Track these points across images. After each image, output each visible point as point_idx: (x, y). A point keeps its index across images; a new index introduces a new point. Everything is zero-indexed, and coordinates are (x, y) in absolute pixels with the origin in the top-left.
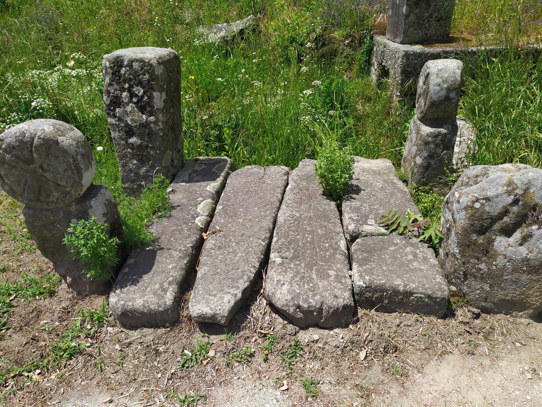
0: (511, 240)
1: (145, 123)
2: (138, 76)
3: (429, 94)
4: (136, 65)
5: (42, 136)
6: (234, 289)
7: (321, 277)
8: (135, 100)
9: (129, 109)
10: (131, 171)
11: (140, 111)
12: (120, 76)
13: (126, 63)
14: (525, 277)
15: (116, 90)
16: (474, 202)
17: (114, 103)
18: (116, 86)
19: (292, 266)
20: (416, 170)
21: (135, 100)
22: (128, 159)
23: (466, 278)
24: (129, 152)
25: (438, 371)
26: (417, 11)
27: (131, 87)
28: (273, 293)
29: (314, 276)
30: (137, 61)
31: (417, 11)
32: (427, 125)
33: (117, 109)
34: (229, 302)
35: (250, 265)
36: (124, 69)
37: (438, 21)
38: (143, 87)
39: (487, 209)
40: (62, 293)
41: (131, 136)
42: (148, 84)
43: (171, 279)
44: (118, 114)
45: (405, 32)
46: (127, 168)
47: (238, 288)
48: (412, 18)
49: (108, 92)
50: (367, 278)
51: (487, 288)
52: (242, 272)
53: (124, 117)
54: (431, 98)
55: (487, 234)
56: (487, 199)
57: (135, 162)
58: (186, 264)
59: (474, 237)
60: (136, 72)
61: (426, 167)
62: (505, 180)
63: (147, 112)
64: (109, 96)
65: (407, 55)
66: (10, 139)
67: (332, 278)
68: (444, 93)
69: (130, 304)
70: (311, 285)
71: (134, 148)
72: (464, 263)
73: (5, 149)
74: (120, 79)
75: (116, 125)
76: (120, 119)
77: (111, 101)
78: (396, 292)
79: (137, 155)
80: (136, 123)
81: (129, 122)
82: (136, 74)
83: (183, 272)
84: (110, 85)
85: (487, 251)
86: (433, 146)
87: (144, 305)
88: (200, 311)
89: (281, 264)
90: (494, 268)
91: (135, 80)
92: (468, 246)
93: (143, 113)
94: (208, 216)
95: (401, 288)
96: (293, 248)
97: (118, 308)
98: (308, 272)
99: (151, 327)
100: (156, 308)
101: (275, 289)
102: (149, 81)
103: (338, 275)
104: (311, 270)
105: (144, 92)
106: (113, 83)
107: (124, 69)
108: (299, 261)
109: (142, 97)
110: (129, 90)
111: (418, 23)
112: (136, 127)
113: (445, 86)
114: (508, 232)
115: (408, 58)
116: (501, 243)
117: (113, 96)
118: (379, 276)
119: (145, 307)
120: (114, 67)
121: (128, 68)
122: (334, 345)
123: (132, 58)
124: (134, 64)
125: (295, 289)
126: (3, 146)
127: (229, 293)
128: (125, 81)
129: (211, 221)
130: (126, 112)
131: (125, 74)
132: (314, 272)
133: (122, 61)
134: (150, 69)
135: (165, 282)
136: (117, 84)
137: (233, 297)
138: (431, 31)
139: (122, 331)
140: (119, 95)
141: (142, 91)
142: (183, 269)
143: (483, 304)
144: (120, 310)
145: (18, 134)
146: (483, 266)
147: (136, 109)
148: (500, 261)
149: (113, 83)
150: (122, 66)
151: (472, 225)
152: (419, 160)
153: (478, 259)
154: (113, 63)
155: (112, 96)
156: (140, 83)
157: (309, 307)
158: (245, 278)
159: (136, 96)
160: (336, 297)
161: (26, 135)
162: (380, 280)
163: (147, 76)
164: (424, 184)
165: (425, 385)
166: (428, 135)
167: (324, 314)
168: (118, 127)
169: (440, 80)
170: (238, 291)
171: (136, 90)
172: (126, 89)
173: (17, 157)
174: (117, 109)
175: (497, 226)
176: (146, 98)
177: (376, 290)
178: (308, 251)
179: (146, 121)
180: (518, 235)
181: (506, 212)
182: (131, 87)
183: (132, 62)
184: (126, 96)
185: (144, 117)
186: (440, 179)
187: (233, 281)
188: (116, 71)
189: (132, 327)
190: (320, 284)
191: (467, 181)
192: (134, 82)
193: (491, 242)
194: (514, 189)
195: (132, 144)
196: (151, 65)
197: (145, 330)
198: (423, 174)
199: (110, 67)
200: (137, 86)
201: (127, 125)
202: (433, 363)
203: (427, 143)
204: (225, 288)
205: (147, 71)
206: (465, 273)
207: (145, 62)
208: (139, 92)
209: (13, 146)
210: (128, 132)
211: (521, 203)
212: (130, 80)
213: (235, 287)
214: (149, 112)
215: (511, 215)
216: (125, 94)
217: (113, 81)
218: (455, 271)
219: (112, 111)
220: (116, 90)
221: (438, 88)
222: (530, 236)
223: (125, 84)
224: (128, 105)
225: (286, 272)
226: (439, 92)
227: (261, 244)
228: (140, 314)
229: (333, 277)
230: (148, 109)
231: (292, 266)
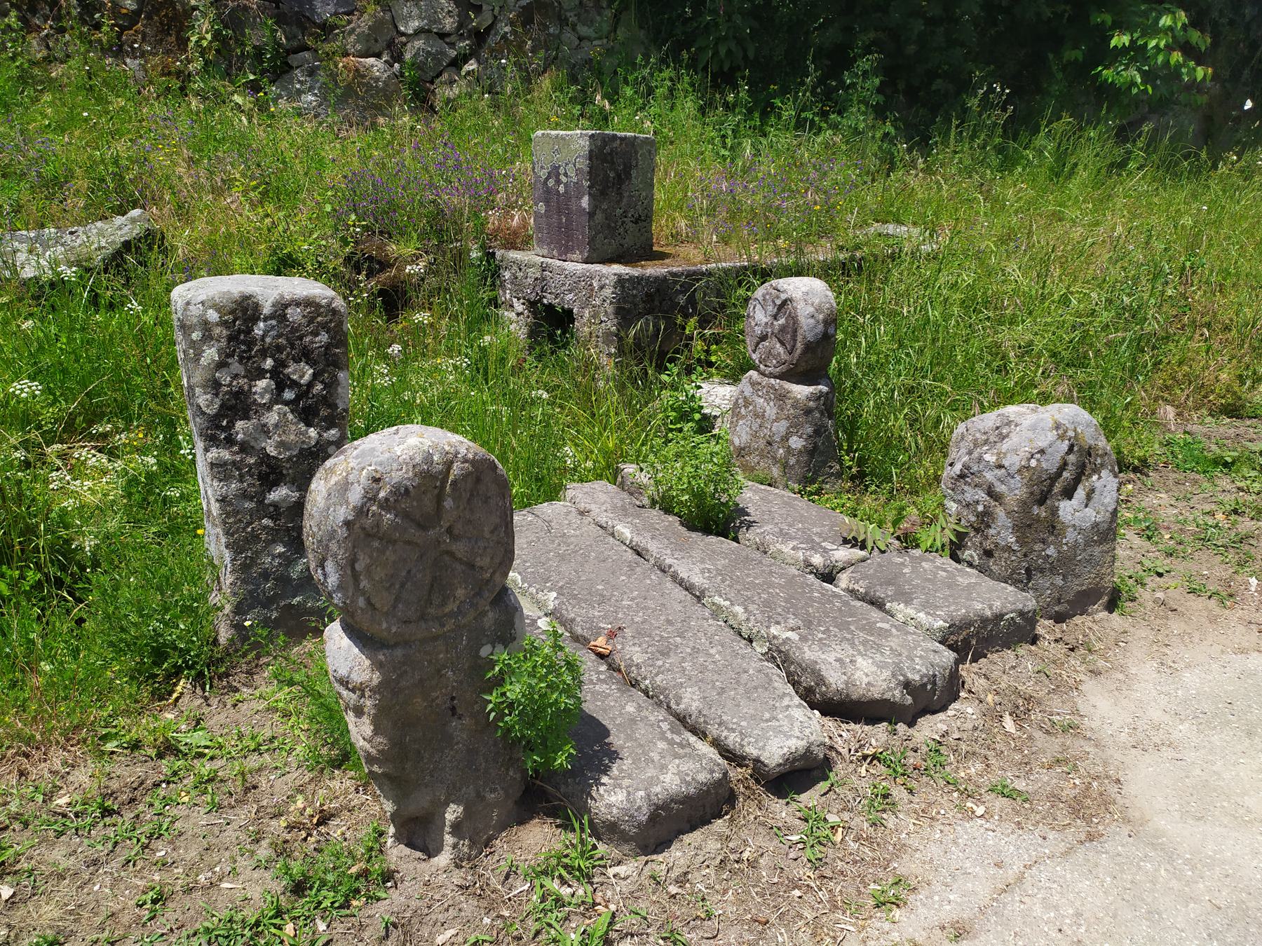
0: (1074, 501)
1: (315, 446)
2: (301, 338)
3: (800, 331)
4: (294, 314)
5: (470, 456)
8: (289, 395)
9: (272, 418)
10: (265, 575)
11: (301, 420)
12: (250, 344)
13: (267, 310)
14: (1097, 550)
15: (236, 376)
16: (1029, 460)
17: (231, 408)
18: (236, 367)
20: (792, 461)
21: (289, 395)
22: (262, 544)
23: (1029, 578)
24: (265, 527)
26: (604, 206)
27: (280, 364)
28: (847, 683)
30: (298, 304)
31: (604, 206)
32: (798, 383)
33: (239, 425)
36: (262, 325)
37: (636, 223)
38: (311, 362)
39: (1044, 465)
40: (411, 866)
41: (275, 484)
42: (326, 354)
44: (240, 436)
45: (592, 241)
46: (255, 571)
48: (599, 217)
49: (215, 385)
51: (1059, 581)
53: (256, 439)
54: (805, 338)
55: (1048, 502)
56: (1042, 452)
57: (280, 549)
59: (1036, 510)
60: (294, 330)
61: (811, 452)
62: (1050, 424)
63: (321, 420)
64: (217, 395)
65: (620, 281)
66: (400, 473)
68: (821, 327)
69: (658, 789)
71: (280, 514)
72: (1025, 555)
73: (387, 500)
74: (250, 350)
75: (234, 463)
76: (245, 448)
77: (221, 406)
78: (984, 621)
79: (288, 529)
80: (289, 449)
81: (271, 451)
82: (294, 335)
84: (221, 365)
85: (1053, 526)
86: (818, 415)
87: (683, 781)
88: (786, 750)
90: (1065, 548)
91: (292, 348)
92: (1029, 526)
93: (309, 425)
95: (988, 613)
97: (639, 808)
99: (693, 829)
100: (709, 776)
101: (844, 674)
102: (328, 347)
105: (315, 375)
106: (230, 361)
107: (262, 325)
109: (310, 385)
110: (275, 373)
111: (609, 226)
112: (289, 459)
113: (821, 317)
114: (1068, 493)
115: (623, 287)
116: (1067, 509)
117: (230, 393)
119: (688, 784)
120: (234, 321)
121: (274, 322)
122: (970, 727)
123: (282, 297)
124: (289, 311)
126: (382, 494)
128: (264, 353)
130: (264, 430)
131: (263, 337)
133: (257, 306)
134: (331, 321)
136: (240, 362)
138: (628, 241)
139: (647, 863)
140: (246, 388)
141: (311, 371)
143: (1057, 608)
144: (645, 810)
145: (418, 459)
146: (1051, 551)
147: (290, 417)
148: (1071, 536)
149: (230, 361)
150: (258, 319)
151: (1032, 493)
152: (796, 443)
153: (1044, 541)
154: (232, 312)
155: (226, 393)
156: (306, 355)
157: (922, 677)
159: (294, 384)
161: (435, 458)
163: (323, 338)
164: (813, 481)
166: (809, 399)
167: (939, 682)
168: (238, 469)
169: (811, 309)
171: (295, 372)
172: (267, 371)
173: (406, 515)
174: (239, 425)
175: (1058, 488)
176: (319, 387)
177: (961, 628)
179: (317, 443)
180: (1080, 493)
181: (1064, 466)
182: (280, 364)
183: (286, 306)
184: (266, 390)
185: (313, 432)
186: (831, 467)
188: (239, 332)
189: (662, 843)
191: (984, 437)
192: (288, 354)
193: (1054, 511)
194: (1066, 432)
195: (275, 505)
196: (334, 312)
197: (687, 838)
198: (808, 464)
199: (224, 324)
200: (297, 361)
201: (265, 458)
202: (1079, 701)
203: (808, 412)
205: (324, 326)
206: (1028, 571)
207: (318, 306)
208: (302, 377)
209: (407, 490)
210: (268, 475)
211: (1076, 449)
212: (279, 349)
214: (325, 419)
215: (1070, 468)
216: (262, 384)
217: (231, 355)
218: (1013, 572)
219: (223, 429)
220: (236, 376)
221: (812, 321)
222: (1093, 491)
223: (265, 359)
224: (269, 409)
226: (815, 327)
228: (681, 803)
230: (324, 412)
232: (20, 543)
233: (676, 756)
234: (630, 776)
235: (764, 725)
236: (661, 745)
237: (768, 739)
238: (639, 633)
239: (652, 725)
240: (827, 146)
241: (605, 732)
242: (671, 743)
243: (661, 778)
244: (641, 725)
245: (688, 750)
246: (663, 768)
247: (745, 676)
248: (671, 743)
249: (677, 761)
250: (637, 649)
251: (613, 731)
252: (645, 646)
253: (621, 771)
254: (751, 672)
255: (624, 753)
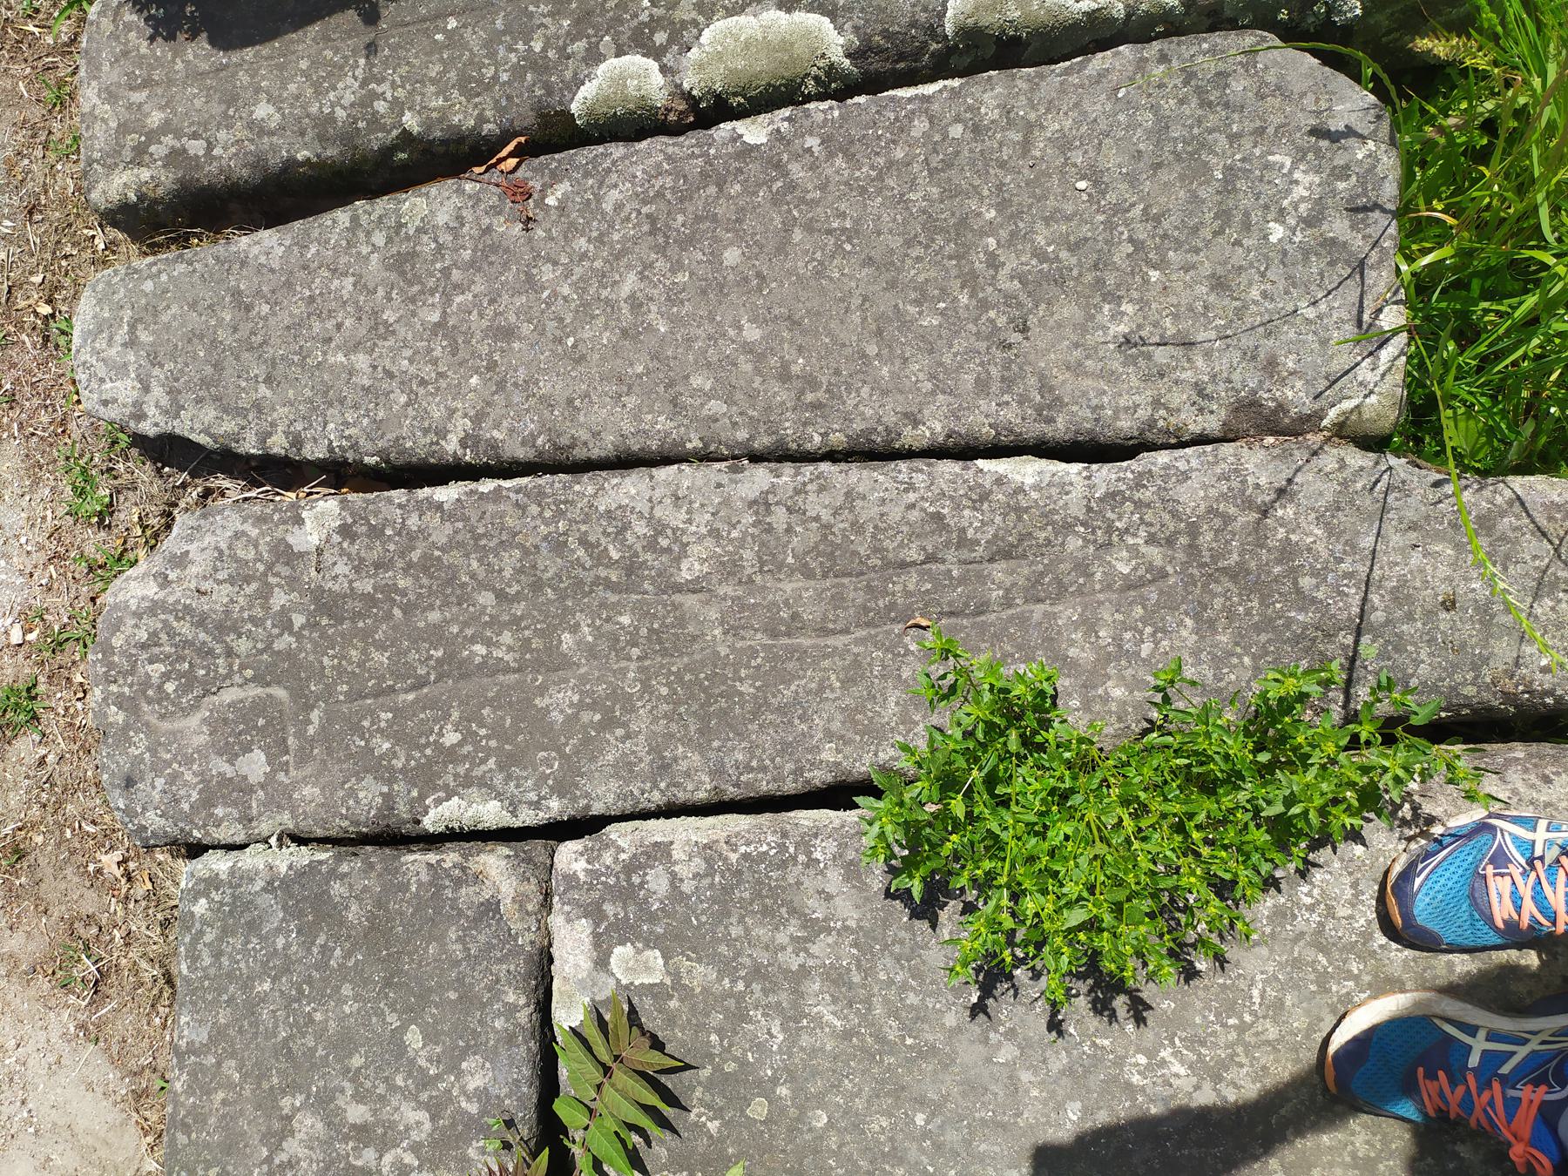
6: (165, 401)
7: (225, 721)
19: (279, 599)
25: (90, 1087)
29: (229, 695)
34: (105, 403)
35: (299, 426)
43: (196, 147)
47: (175, 410)
50: (200, 908)
52: (258, 407)
58: (291, 163)
67: (220, 766)
70: (170, 687)
83: (245, 173)
89: (285, 554)
94: (688, 96)
96: (390, 589)
98: (243, 667)
103: (251, 790)
104: (254, 679)
108: (312, 625)
118: (217, 955)
125: (128, 629)
127: (146, 389)
129: (676, 130)
132: (255, 691)
135: (178, 137)
137: (127, 411)
142: (258, 163)
158: (228, 426)
160: (129, 783)
162: (194, 958)
165: (42, 1036)
170: (160, 419)
178: (381, 658)
187: (205, 383)
190: (194, 721)
204: (169, 366)
213: (174, 401)
225: (240, 578)
227: (442, 433)
229: (229, 771)
231: (279, 599)
232: (779, 1004)
233: (123, 128)
234: (114, 36)
235: (127, 314)
236: (156, 118)
237: (99, 301)
238: (490, 250)
239: (205, 125)
240: (916, 423)
241: (225, 39)
242: (153, 136)
243: (94, 83)
244: (217, 109)
245: (127, 154)
246: (110, 96)
247: (258, 370)
248: (153, 136)
249: (114, 125)
250: (442, 218)
251: (222, 57)
252: (446, 238)
253: (128, 27)
254: (263, 390)
255: (161, 49)
